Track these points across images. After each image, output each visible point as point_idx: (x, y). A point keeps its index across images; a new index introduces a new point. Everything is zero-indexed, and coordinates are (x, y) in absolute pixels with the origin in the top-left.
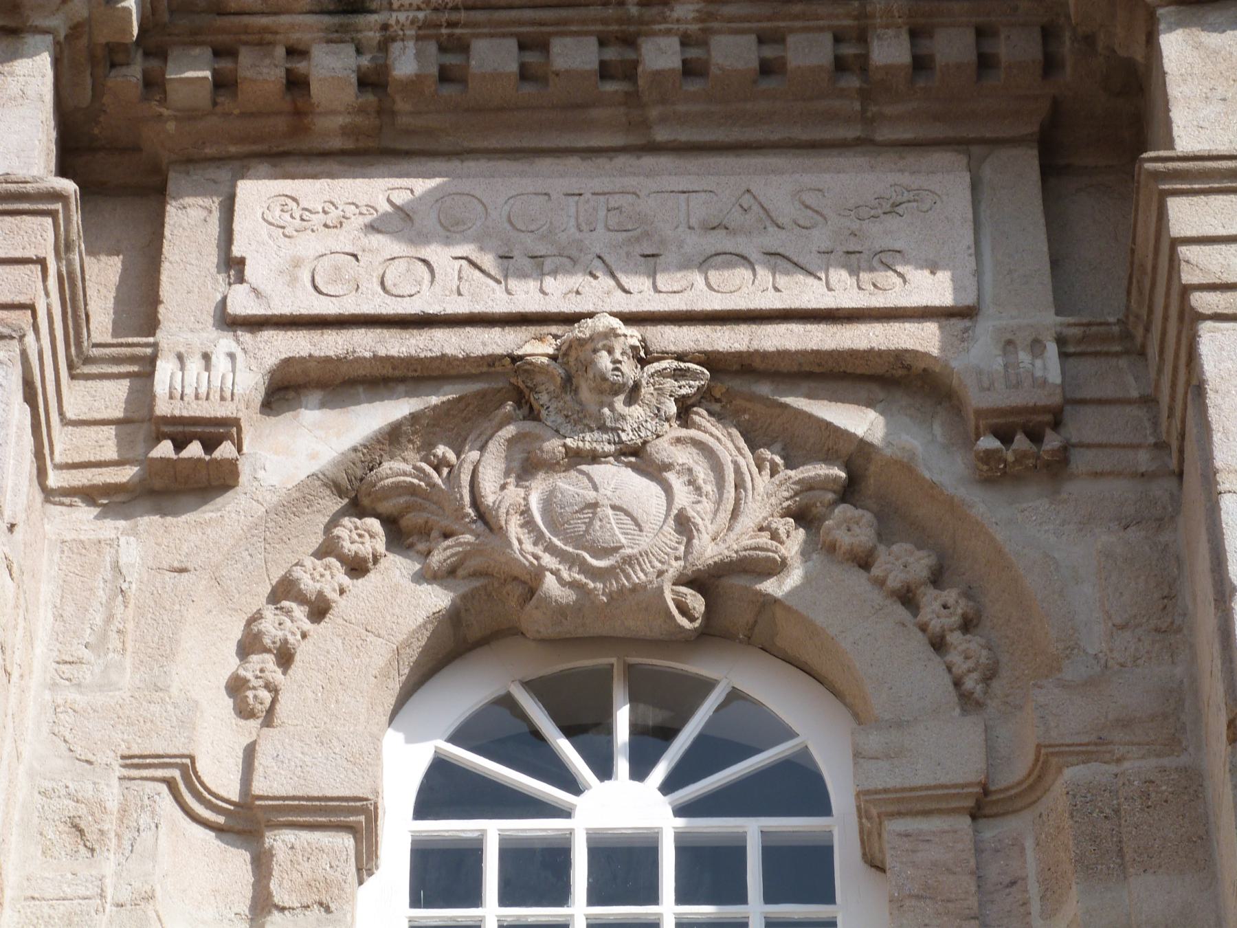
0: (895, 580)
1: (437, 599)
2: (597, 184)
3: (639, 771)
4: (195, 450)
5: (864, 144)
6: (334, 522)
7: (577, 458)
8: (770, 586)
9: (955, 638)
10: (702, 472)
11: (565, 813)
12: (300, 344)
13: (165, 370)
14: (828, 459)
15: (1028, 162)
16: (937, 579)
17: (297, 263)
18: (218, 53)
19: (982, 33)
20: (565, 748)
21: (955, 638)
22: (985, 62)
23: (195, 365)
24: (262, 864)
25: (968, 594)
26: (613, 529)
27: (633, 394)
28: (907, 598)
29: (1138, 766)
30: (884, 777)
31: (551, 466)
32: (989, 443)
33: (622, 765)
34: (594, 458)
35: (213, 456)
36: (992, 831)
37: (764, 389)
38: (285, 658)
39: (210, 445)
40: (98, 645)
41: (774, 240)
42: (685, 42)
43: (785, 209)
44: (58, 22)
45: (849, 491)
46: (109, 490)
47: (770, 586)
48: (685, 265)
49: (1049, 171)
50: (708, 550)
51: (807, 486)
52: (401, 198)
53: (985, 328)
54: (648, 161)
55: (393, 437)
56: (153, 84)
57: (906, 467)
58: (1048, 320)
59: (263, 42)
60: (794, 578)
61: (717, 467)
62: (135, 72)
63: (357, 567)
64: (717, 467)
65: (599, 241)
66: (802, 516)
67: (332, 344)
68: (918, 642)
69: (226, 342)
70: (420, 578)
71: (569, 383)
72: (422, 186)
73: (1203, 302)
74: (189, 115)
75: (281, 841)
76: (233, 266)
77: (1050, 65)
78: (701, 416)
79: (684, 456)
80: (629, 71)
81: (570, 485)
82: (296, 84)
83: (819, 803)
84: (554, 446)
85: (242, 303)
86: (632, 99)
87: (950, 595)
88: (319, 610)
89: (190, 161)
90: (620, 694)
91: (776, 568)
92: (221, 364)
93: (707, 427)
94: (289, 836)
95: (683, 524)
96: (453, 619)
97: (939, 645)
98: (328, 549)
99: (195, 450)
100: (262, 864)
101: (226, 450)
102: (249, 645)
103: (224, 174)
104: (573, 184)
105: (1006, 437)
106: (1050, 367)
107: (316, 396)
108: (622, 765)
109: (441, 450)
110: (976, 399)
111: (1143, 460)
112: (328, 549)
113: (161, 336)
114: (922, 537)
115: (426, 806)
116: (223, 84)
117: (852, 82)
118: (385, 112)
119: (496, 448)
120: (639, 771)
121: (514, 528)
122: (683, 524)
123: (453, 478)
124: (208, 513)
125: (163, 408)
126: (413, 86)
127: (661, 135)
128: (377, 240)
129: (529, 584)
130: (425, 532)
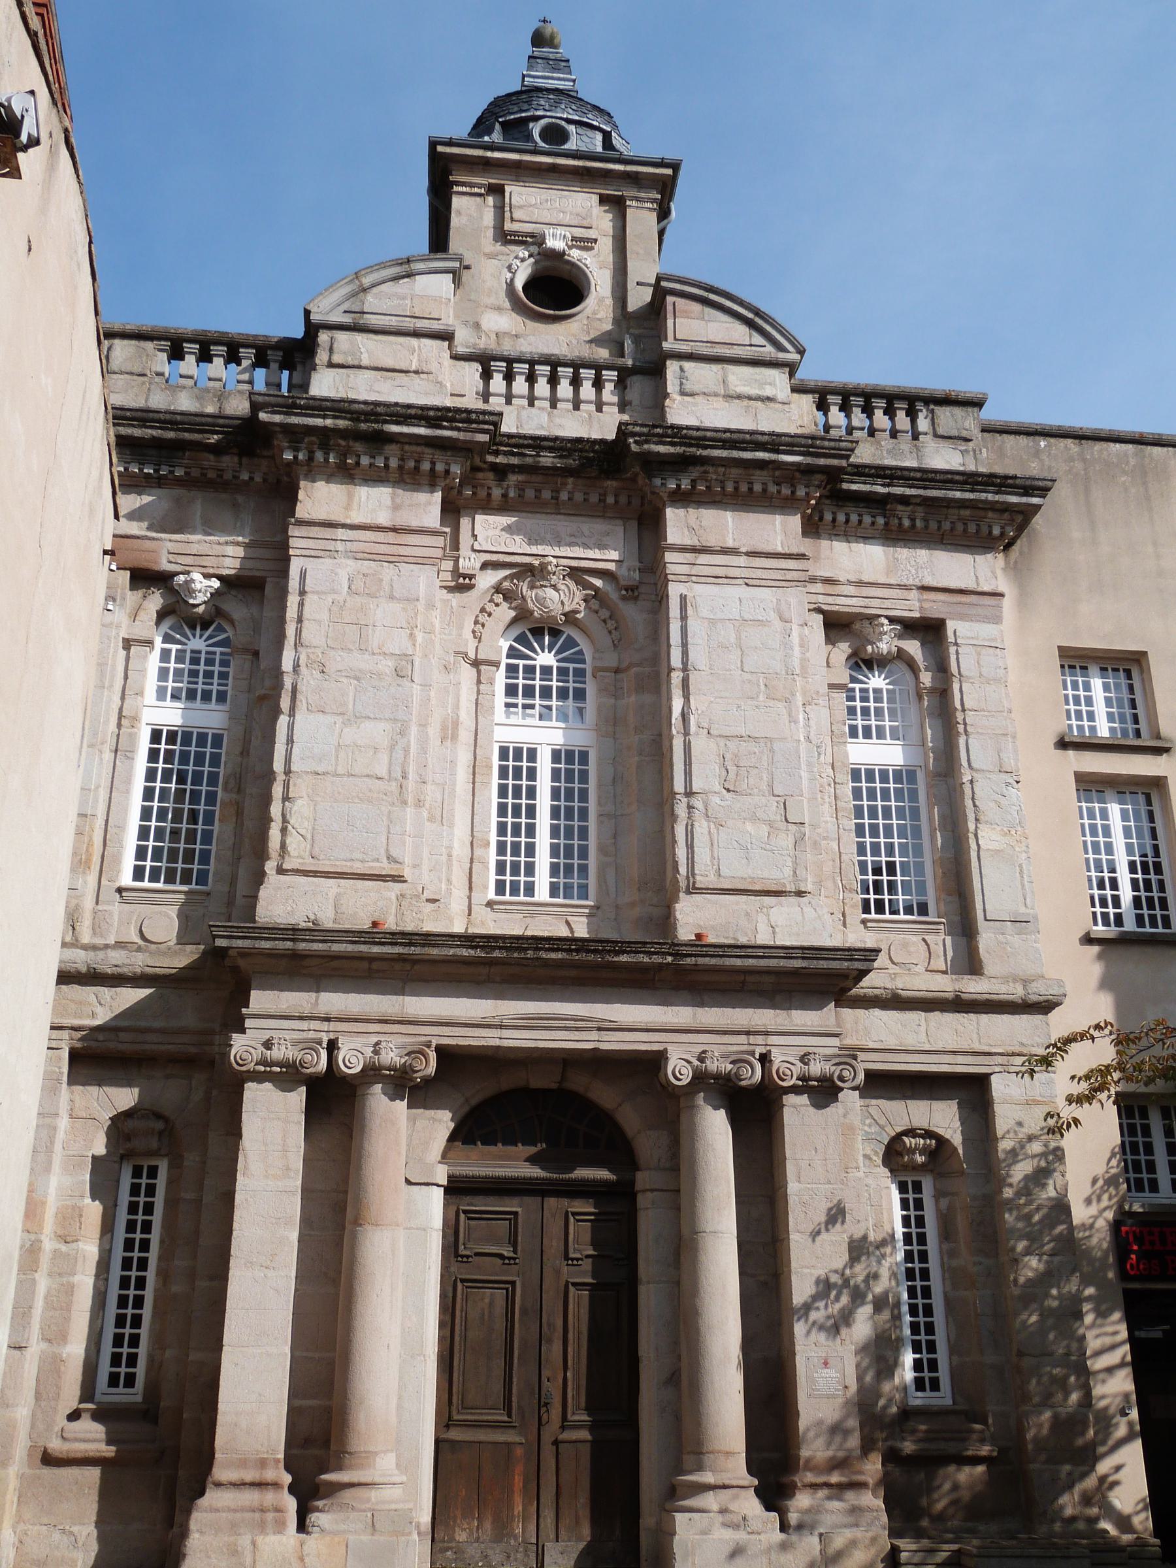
0: (603, 618)
1: (513, 614)
2: (549, 522)
3: (550, 652)
4: (467, 581)
5: (603, 517)
6: (493, 595)
7: (542, 586)
8: (578, 616)
9: (613, 631)
10: (566, 591)
11: (535, 660)
12: (488, 557)
13: (461, 560)
14: (592, 590)
15: (635, 524)
16: (610, 617)
17: (488, 537)
18: (473, 487)
19: (629, 496)
20: (535, 645)
21: (613, 631)
22: (629, 503)
23: (467, 560)
24: (479, 672)
25: (617, 622)
26: (549, 603)
27: (554, 574)
28: (605, 621)
29: (647, 670)
30: (599, 664)
31: (537, 588)
32: (624, 592)
33: (546, 650)
34: (545, 586)
35: (897, 1380)
36: (619, 676)
37: (580, 573)
38: (483, 625)
39: (470, 580)
40: (448, 625)
41: (584, 540)
42: (569, 492)
43: (587, 533)
44: (443, 484)
45: (594, 597)
46: (449, 587)
47: (578, 616)
48: (566, 545)
49: (639, 524)
50: (567, 609)
51: (586, 595)
52: (509, 522)
53: (625, 564)
54: (559, 516)
55: (506, 578)
56: (460, 493)
57: (607, 594)
58: (637, 564)
59: (482, 486)
60: (582, 615)
61: (569, 590)
62: (456, 491)
63: (497, 605)
64: (569, 590)
65: (549, 536)
66: (585, 600)
67: (495, 557)
68: (606, 632)
69: (473, 555)
70: (509, 608)
71: (542, 570)
72: (514, 519)
73: (670, 577)
74: (466, 499)
75: (483, 668)
76: (475, 536)
77: (642, 505)
78: (567, 578)
79: (563, 587)
80: (557, 498)
81: (540, 592)
82: (489, 495)
83: (583, 662)
84: (538, 583)
85: (476, 547)
86: (557, 504)
87: (618, 633)
88: (490, 615)
89: (465, 508)
90: (546, 633)
91: (579, 612)
92: (472, 560)
93: (569, 581)
94: (484, 667)
95: (562, 603)
96: (515, 617)
97: (610, 632)
98: (491, 601)
99: (467, 581)
100: (479, 672)
101: (473, 581)
102: (476, 622)
103: (472, 512)
104: (543, 522)
105: (626, 590)
106: (637, 575)
107: (490, 567)
108: (546, 650)
109: (515, 581)
110: (622, 582)
111: (653, 597)
112: (491, 601)
113: (460, 552)
114: (608, 608)
115: (508, 657)
116: (474, 493)
117: (602, 504)
118: (506, 502)
119: (526, 582)
120: (550, 652)
121: (529, 601)
122: (562, 603)
123: (517, 588)
124: (469, 594)
125: (461, 571)
126: (512, 498)
127: (562, 511)
128: (503, 533)
129: (532, 613)
130: (511, 598)
